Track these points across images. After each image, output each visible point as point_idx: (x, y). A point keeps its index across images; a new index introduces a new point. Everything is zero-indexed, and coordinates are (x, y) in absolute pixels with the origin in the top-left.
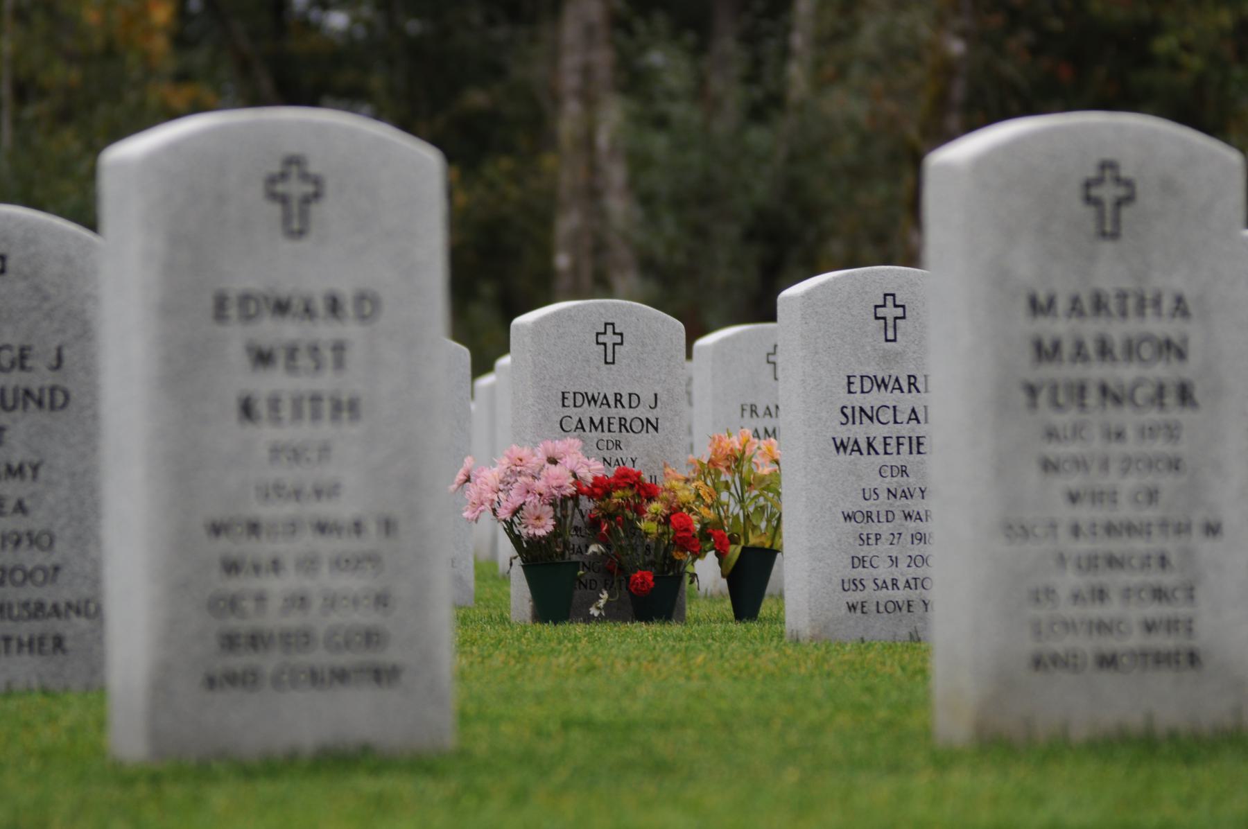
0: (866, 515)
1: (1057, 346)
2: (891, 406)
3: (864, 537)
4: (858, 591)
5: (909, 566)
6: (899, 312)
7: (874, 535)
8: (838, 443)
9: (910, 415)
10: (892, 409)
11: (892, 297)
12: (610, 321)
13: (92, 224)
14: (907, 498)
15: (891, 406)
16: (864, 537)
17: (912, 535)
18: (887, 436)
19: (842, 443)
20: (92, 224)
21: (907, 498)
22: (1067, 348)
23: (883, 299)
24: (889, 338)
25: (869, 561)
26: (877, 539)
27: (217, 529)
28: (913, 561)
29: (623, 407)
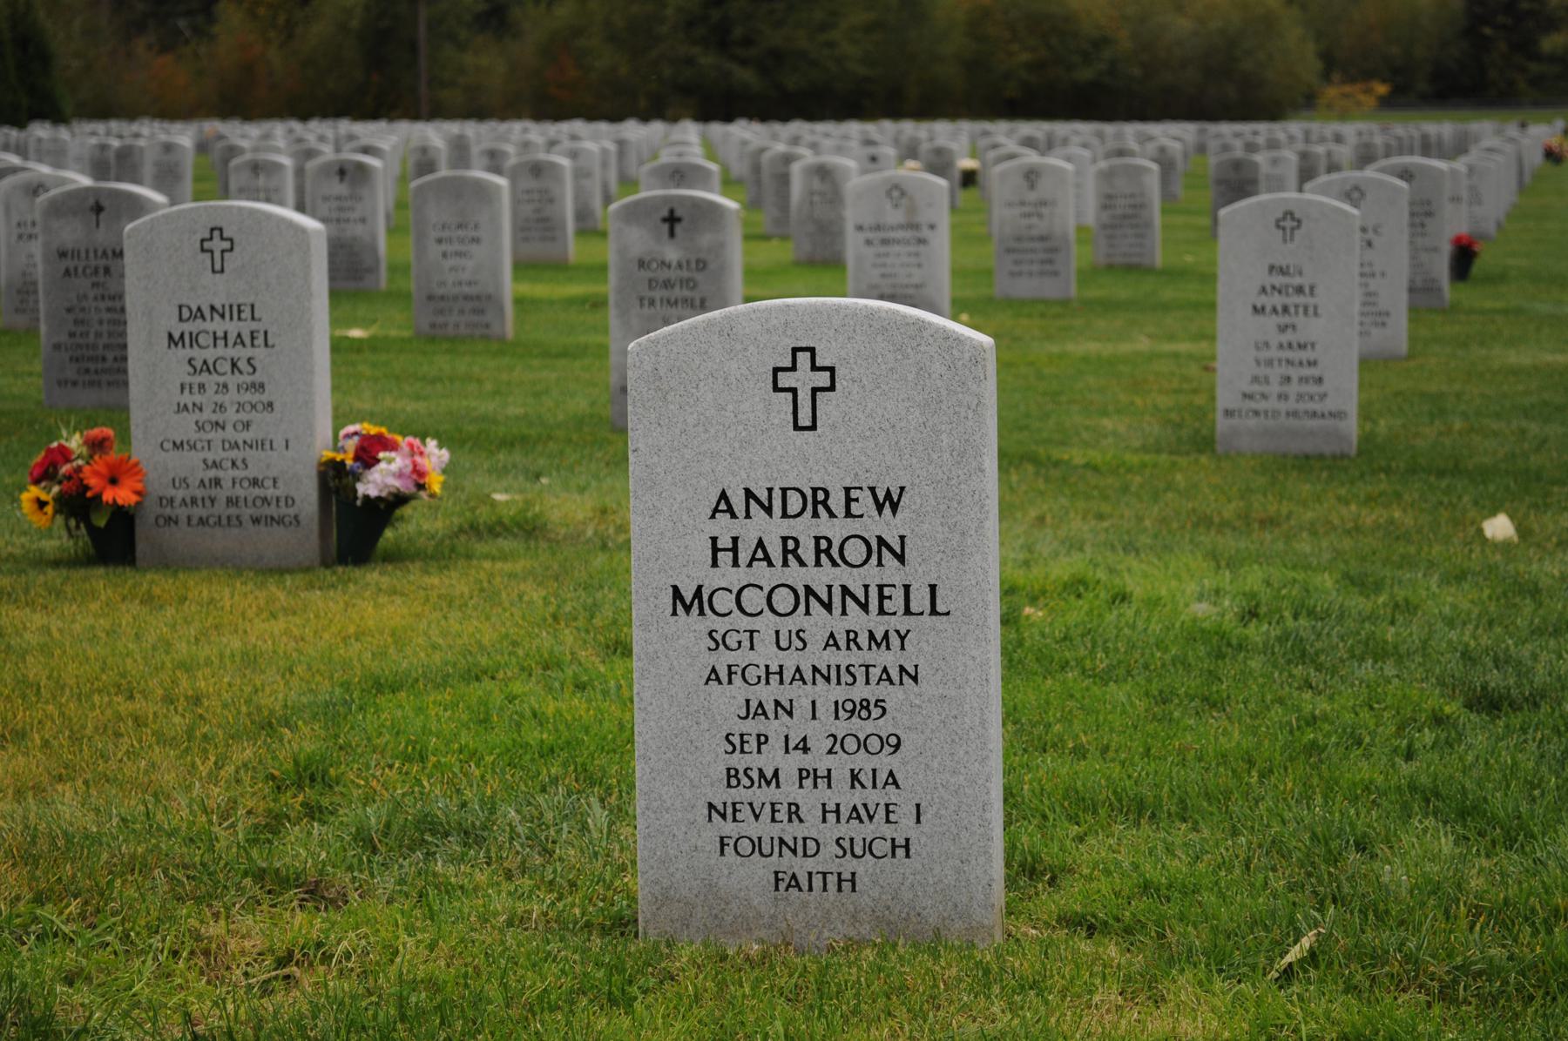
0: (810, 499)
1: (1263, 308)
2: (889, 837)
3: (736, 740)
4: (741, 787)
5: (830, 752)
6: (823, 379)
7: (754, 736)
8: (881, 496)
9: (755, 552)
10: (889, 841)
11: (808, 354)
12: (218, 275)
13: (724, 491)
14: (861, 821)
15: (889, 837)
16: (736, 740)
17: (836, 703)
18: (854, 485)
19: (888, 494)
20: (724, 491)
21: (861, 821)
22: (1268, 309)
23: (790, 358)
24: (801, 423)
25: (732, 844)
26: (759, 744)
28: (838, 745)
29: (832, 515)
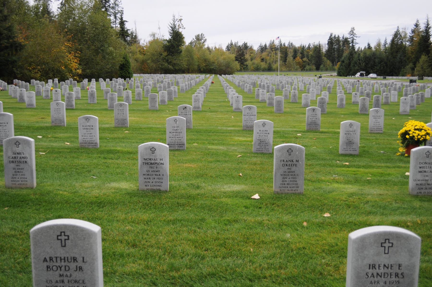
27: (144, 175)
